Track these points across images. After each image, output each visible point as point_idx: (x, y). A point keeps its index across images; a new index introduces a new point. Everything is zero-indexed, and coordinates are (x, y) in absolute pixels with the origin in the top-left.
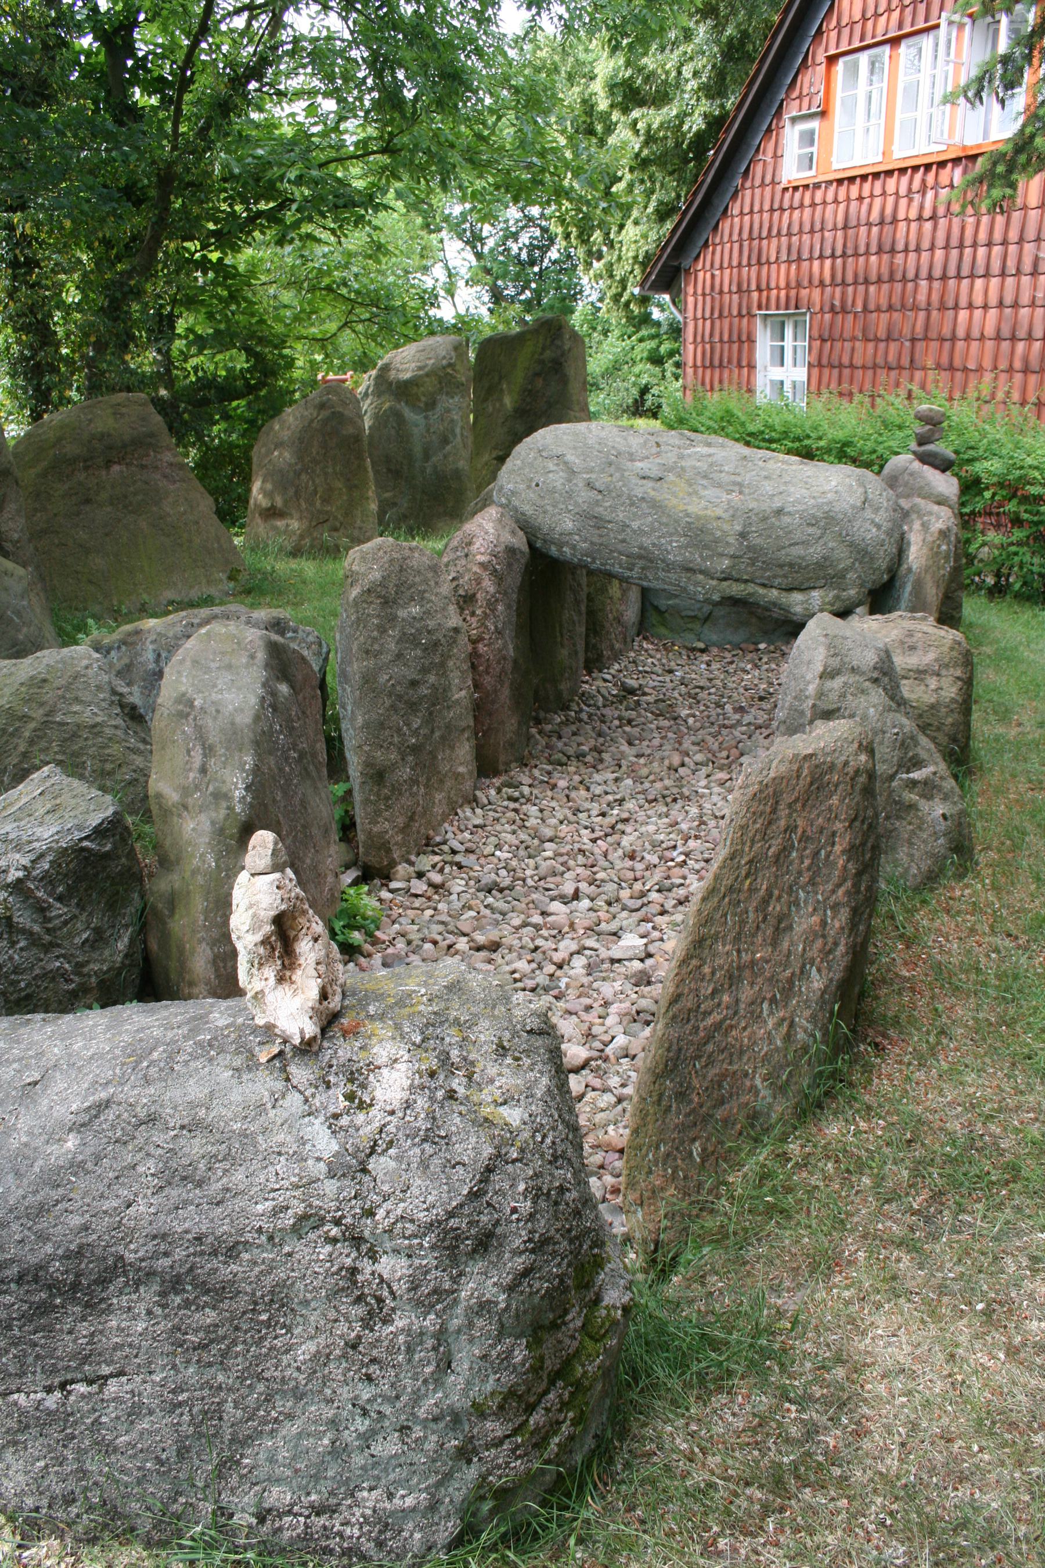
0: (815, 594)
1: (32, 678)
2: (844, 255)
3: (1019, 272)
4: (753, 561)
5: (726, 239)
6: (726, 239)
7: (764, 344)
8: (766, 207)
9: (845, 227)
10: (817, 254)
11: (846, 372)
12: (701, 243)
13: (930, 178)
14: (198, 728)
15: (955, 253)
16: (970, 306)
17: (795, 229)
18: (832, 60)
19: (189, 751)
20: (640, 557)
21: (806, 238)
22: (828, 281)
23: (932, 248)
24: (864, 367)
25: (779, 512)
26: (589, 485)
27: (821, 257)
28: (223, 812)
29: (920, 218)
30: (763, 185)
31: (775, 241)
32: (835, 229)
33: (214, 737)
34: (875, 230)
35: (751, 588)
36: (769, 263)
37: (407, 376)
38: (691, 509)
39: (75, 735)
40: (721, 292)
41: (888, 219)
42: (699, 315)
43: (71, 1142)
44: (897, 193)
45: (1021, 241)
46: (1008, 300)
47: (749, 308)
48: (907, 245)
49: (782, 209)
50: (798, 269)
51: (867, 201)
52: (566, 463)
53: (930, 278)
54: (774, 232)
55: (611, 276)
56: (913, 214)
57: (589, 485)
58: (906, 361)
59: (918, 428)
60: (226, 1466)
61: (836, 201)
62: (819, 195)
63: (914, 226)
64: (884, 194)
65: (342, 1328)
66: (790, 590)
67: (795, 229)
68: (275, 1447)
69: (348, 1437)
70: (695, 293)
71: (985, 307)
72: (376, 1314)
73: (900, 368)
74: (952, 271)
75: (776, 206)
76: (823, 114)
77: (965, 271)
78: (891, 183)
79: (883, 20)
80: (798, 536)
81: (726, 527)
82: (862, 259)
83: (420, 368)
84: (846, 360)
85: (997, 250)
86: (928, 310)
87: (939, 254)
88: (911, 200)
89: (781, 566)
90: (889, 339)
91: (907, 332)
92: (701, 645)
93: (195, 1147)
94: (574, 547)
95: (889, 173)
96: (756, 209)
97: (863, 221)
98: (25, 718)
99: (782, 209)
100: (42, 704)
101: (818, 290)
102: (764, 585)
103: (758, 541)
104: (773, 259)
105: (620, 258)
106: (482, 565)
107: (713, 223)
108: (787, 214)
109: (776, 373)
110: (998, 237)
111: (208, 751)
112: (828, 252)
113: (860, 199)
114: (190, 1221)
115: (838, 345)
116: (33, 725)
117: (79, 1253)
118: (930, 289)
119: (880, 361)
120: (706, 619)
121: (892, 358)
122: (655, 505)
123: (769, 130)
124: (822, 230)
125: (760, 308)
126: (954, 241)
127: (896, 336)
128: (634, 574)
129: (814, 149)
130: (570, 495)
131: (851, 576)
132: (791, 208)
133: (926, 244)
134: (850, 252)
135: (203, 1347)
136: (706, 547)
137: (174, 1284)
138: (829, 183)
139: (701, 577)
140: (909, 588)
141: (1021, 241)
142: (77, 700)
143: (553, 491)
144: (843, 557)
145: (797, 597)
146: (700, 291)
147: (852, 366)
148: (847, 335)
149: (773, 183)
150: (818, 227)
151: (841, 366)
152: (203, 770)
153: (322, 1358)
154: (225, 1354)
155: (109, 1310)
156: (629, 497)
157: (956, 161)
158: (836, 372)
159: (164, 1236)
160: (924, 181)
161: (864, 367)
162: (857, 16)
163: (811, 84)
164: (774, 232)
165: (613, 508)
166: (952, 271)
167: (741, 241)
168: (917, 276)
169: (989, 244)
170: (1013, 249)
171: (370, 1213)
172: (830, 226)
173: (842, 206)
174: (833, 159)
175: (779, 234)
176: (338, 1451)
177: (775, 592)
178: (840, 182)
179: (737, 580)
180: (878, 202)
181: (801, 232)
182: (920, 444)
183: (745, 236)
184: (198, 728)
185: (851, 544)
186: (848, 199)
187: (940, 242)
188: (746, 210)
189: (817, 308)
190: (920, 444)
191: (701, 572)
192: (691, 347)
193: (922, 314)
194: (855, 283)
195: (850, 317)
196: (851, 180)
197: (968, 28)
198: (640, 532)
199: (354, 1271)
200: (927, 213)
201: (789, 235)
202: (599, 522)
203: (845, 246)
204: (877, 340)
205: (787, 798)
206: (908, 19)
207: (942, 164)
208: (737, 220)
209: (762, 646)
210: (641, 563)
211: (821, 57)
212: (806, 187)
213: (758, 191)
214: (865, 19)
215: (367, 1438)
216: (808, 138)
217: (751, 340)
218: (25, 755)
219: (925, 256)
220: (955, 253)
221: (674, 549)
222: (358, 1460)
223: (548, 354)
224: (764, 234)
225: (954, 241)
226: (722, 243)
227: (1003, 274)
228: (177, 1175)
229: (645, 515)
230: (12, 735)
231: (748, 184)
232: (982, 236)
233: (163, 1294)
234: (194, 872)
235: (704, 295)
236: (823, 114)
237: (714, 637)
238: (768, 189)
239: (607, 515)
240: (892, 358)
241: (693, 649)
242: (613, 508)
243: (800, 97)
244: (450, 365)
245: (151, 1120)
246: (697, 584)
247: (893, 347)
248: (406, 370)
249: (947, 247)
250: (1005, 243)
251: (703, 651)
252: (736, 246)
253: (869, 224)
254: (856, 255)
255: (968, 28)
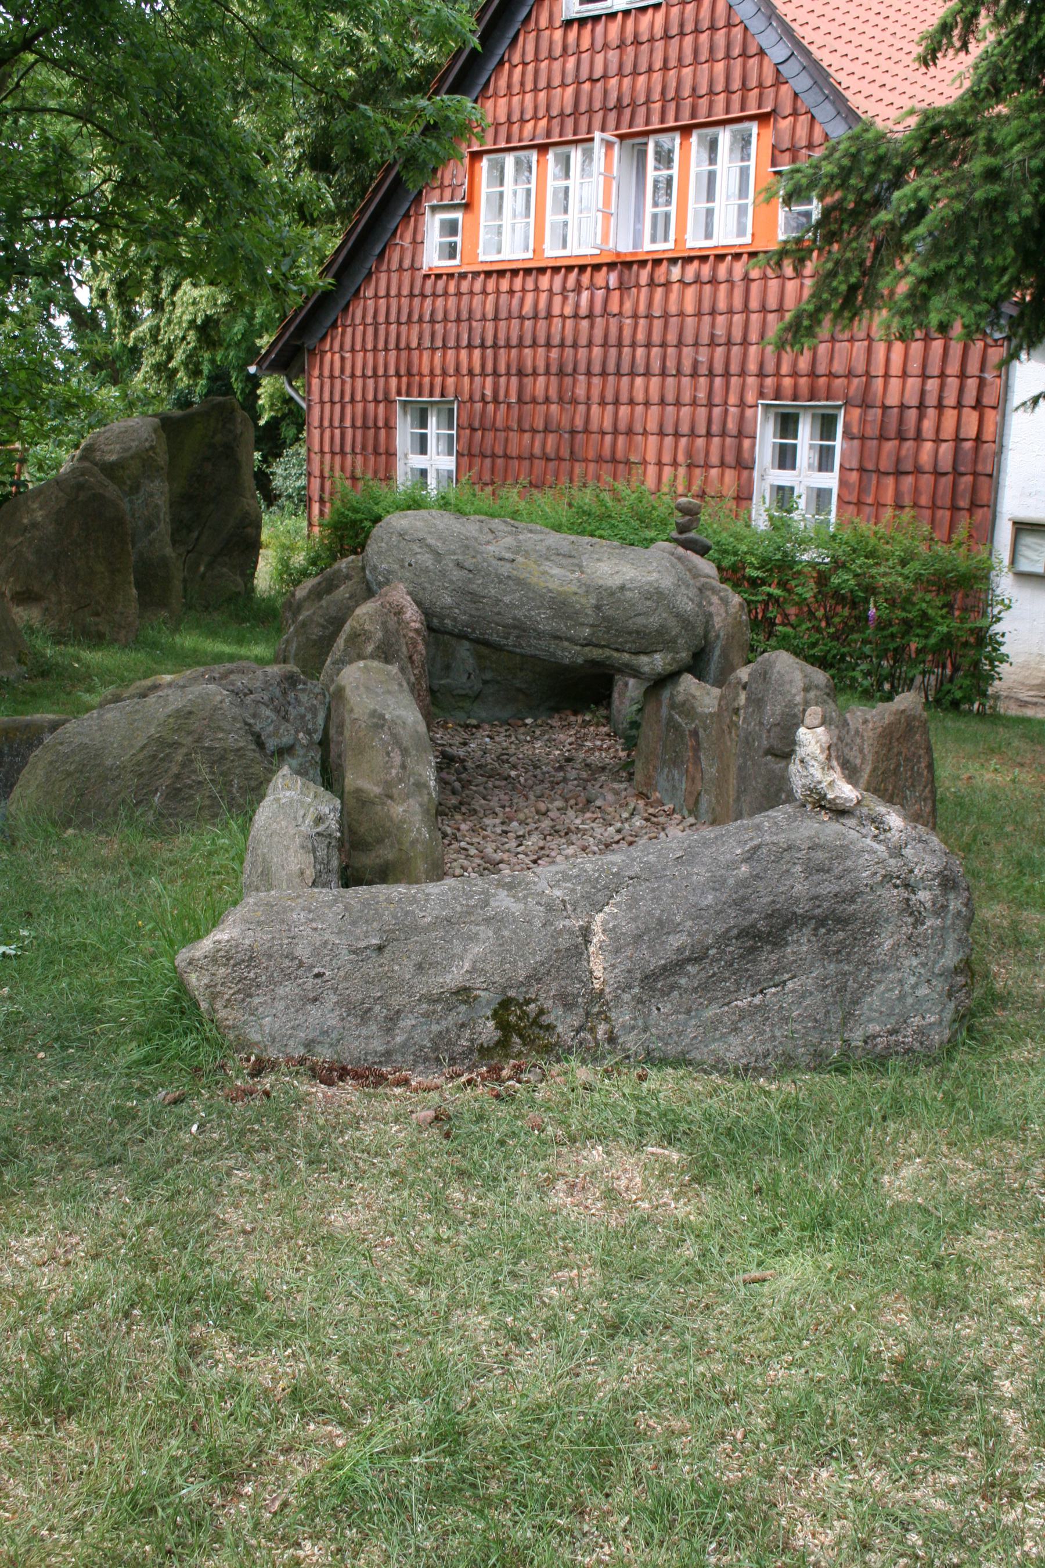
0: (657, 656)
1: (178, 711)
2: (495, 346)
3: (679, 373)
4: (608, 629)
5: (358, 321)
6: (358, 321)
7: (404, 432)
8: (405, 291)
9: (496, 319)
10: (465, 343)
11: (500, 462)
12: (329, 323)
13: (585, 279)
14: (394, 736)
15: (613, 351)
16: (632, 402)
17: (440, 316)
18: (476, 156)
19: (388, 754)
20: (515, 627)
21: (452, 327)
22: (477, 369)
23: (590, 345)
24: (520, 458)
25: (622, 588)
26: (459, 565)
27: (470, 346)
28: (426, 798)
29: (576, 316)
30: (401, 269)
31: (416, 328)
32: (484, 319)
33: (407, 742)
34: (528, 324)
35: (608, 652)
36: (408, 348)
37: (113, 458)
38: (551, 586)
39: (223, 758)
40: (353, 376)
41: (542, 314)
42: (326, 397)
43: (744, 868)
44: (550, 290)
45: (680, 345)
46: (670, 398)
47: (387, 392)
48: (563, 339)
49: (423, 296)
50: (444, 356)
51: (518, 295)
52: (429, 546)
53: (589, 373)
54: (416, 318)
55: (156, 342)
56: (568, 311)
57: (459, 565)
58: (565, 453)
59: (678, 517)
60: (848, 1016)
61: (484, 292)
62: (465, 286)
63: (569, 323)
64: (537, 289)
65: (904, 929)
66: (637, 653)
67: (440, 316)
68: (873, 1000)
69: (907, 988)
70: (321, 376)
71: (647, 404)
72: (919, 922)
73: (559, 459)
74: (611, 368)
75: (417, 292)
76: (467, 206)
77: (625, 368)
78: (544, 281)
79: (529, 126)
80: (640, 608)
81: (583, 601)
82: (514, 351)
83: (125, 450)
84: (499, 451)
85: (655, 351)
86: (588, 405)
87: (597, 351)
88: (565, 298)
89: (630, 633)
90: (546, 430)
91: (565, 423)
92: (474, 722)
93: (820, 855)
94: (455, 619)
95: (542, 270)
96: (393, 293)
97: (515, 314)
98: (176, 745)
99: (423, 296)
100: (189, 733)
101: (466, 379)
102: (617, 650)
103: (611, 612)
104: (414, 345)
105: (169, 322)
106: (416, 630)
107: (344, 303)
108: (429, 301)
109: (418, 461)
110: (656, 338)
111: (405, 752)
112: (477, 342)
113: (511, 292)
114: (828, 888)
115: (490, 435)
116: (184, 750)
117: (771, 916)
118: (589, 384)
119: (537, 451)
120: (477, 697)
121: (550, 449)
122: (520, 582)
123: (407, 216)
124: (470, 319)
125: (399, 394)
126: (613, 339)
127: (554, 427)
128: (510, 641)
129: (458, 239)
130: (443, 574)
131: (681, 641)
132: (434, 295)
133: (583, 341)
134: (502, 343)
135: (839, 952)
136: (569, 618)
137: (822, 922)
138: (476, 274)
139: (566, 644)
140: (717, 652)
141: (680, 345)
142: (220, 729)
143: (426, 571)
144: (675, 628)
145: (644, 659)
146: (326, 373)
147: (506, 456)
148: (499, 424)
149: (413, 268)
150: (465, 315)
151: (494, 456)
152: (403, 767)
153: (896, 946)
154: (848, 954)
155: (787, 944)
156: (497, 576)
157: (611, 266)
158: (488, 462)
159: (817, 898)
160: (578, 282)
161: (520, 458)
162: (503, 119)
163: (454, 176)
164: (416, 318)
165: (485, 586)
166: (611, 368)
167: (376, 324)
168: (575, 370)
169: (648, 345)
170: (671, 351)
171: (911, 871)
172: (478, 316)
173: (491, 298)
174: (480, 251)
175: (421, 320)
176: (902, 998)
177: (626, 656)
178: (488, 274)
179: (596, 646)
180: (530, 298)
181: (445, 319)
182: (681, 532)
183: (381, 319)
184: (394, 736)
185: (678, 615)
186: (498, 292)
187: (598, 339)
188: (382, 292)
189: (466, 397)
190: (681, 532)
191: (567, 639)
192: (316, 433)
193: (582, 408)
194: (508, 374)
195: (503, 407)
196: (501, 273)
197: (616, 147)
198: (511, 606)
199: (908, 900)
200: (583, 311)
201: (433, 321)
202: (475, 598)
203: (495, 336)
204: (534, 431)
205: (896, 735)
206: (556, 130)
207: (597, 267)
208: (370, 303)
209: (529, 721)
210: (516, 632)
211: (465, 151)
212: (451, 276)
213: (395, 276)
214: (510, 122)
215: (915, 987)
216: (451, 228)
217: (389, 427)
218: (178, 776)
219: (582, 353)
220: (613, 351)
221: (543, 620)
222: (910, 1000)
223: (218, 438)
224: (404, 319)
225: (613, 339)
226: (354, 326)
227: (663, 374)
228: (815, 869)
229: (514, 592)
230: (162, 760)
231: (384, 267)
232: (641, 337)
233: (816, 929)
234: (413, 843)
235: (332, 377)
236: (467, 206)
237: (483, 715)
238: (407, 275)
239: (479, 590)
240: (550, 449)
241: (467, 726)
242: (485, 586)
243: (442, 187)
244: (152, 448)
245: (789, 848)
246: (564, 649)
247: (551, 439)
248: (111, 452)
249: (605, 345)
250: (663, 345)
251: (477, 727)
252: (370, 330)
253: (522, 318)
254: (508, 346)
255: (616, 147)
